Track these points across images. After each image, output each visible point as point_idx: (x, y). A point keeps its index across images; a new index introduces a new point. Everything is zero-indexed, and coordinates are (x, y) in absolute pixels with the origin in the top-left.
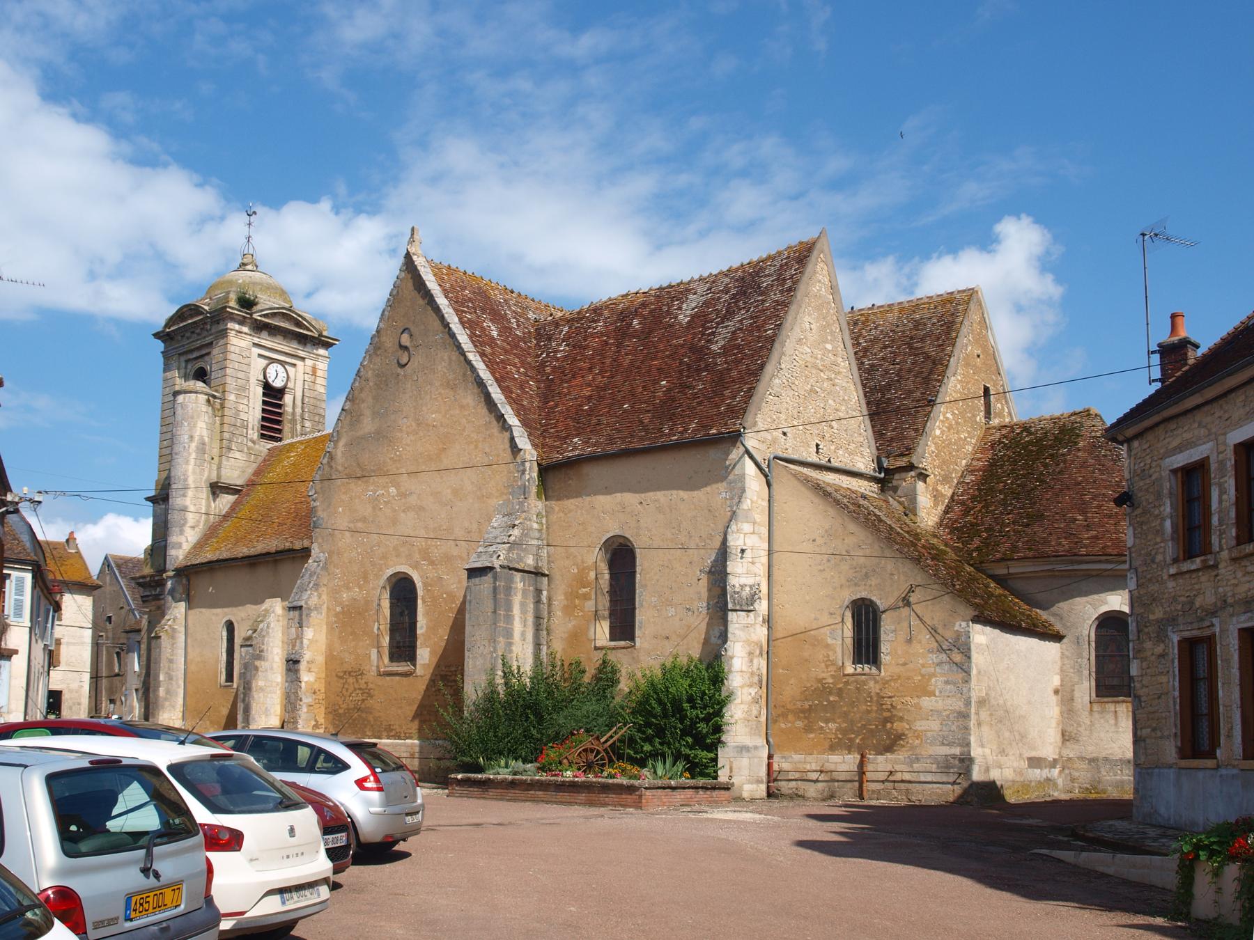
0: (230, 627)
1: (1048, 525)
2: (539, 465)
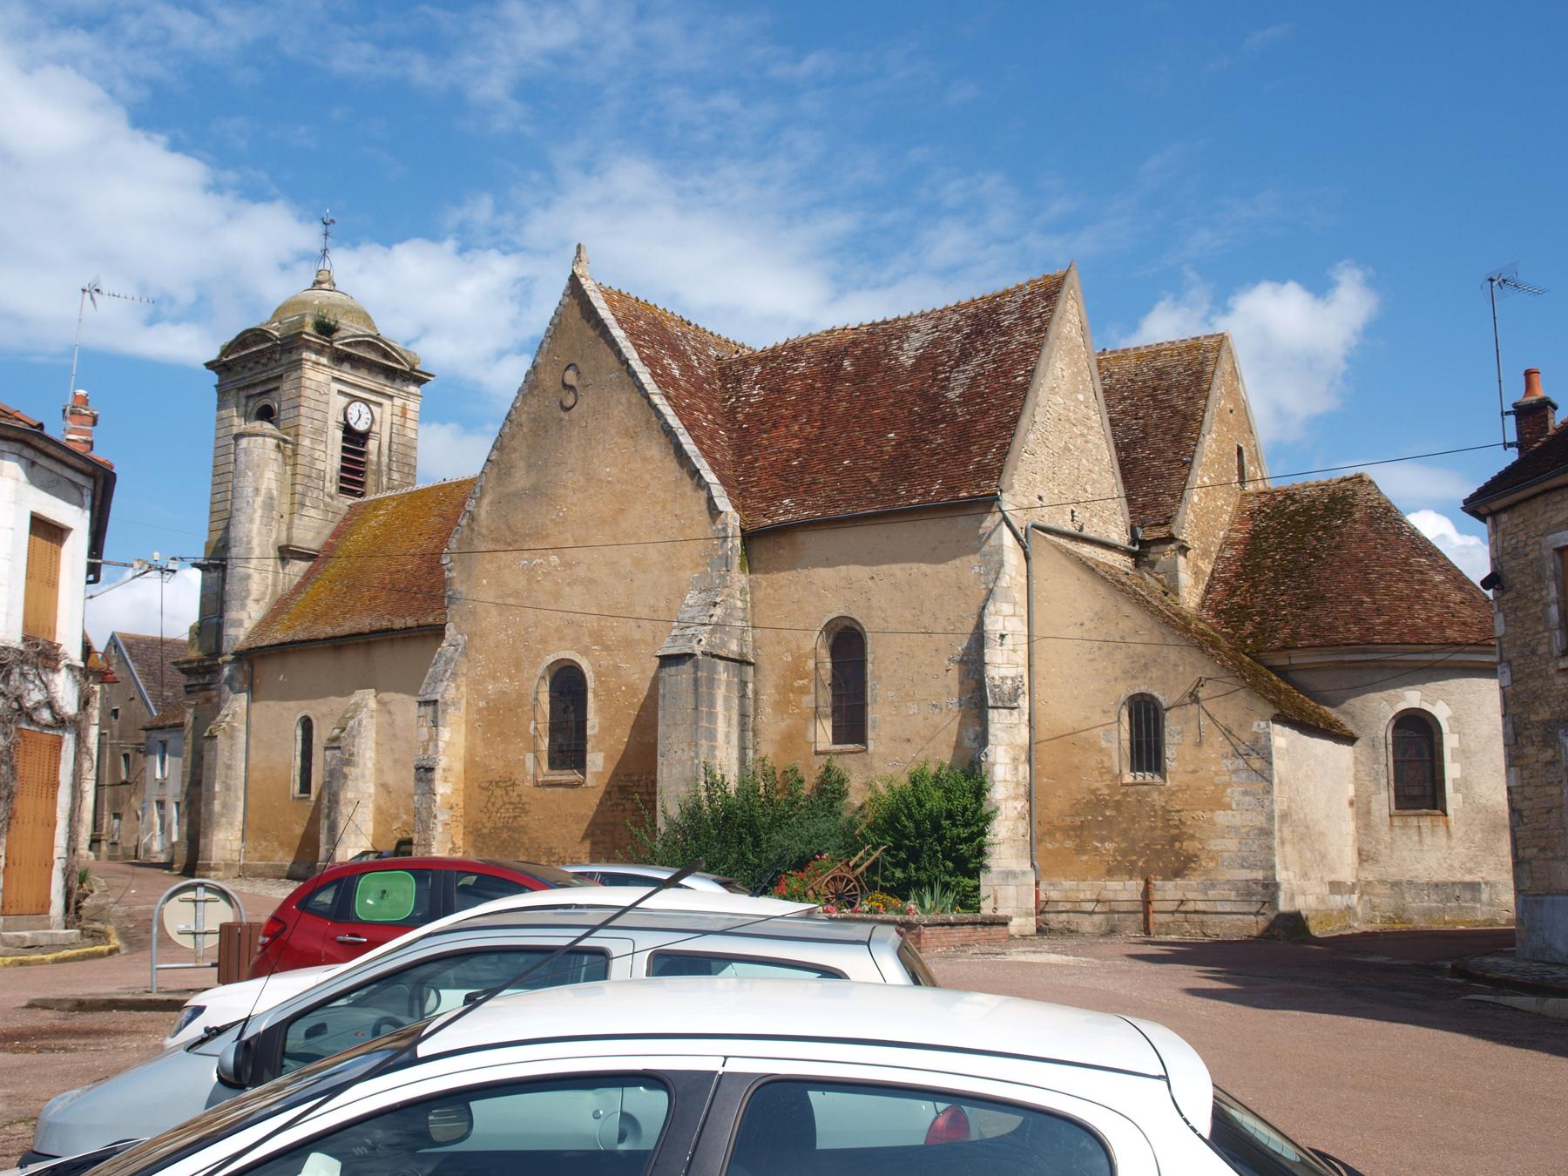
0: (307, 725)
1: (1332, 608)
2: (742, 530)
